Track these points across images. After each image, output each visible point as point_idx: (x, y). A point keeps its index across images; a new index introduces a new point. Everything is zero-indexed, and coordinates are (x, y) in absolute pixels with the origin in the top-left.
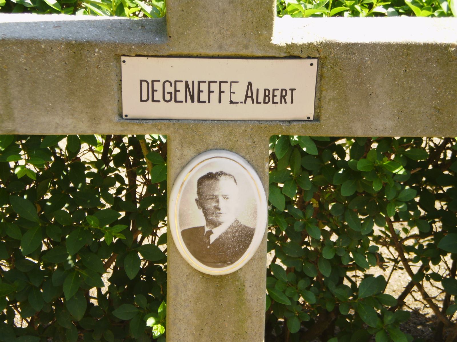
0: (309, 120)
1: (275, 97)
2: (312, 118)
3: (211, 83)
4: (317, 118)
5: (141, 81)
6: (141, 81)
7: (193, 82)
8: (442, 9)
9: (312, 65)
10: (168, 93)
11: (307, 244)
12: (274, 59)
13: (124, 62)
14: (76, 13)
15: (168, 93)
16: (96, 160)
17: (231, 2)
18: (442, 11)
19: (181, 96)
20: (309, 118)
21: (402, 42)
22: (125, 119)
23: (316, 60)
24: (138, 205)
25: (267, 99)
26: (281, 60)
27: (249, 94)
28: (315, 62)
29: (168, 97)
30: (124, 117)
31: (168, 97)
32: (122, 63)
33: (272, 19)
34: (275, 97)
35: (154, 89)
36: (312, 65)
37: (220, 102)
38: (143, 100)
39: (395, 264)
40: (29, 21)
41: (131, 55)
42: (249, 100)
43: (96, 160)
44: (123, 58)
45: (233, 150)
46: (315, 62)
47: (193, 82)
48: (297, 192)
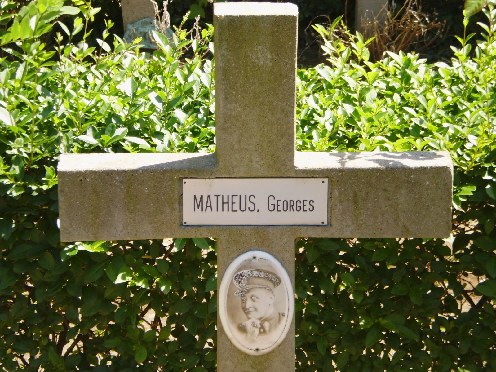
2: (326, 223)
4: (330, 224)
9: (323, 182)
10: (272, 204)
15: (272, 204)
17: (495, 139)
20: (323, 223)
21: (328, 167)
22: (185, 226)
24: (418, 277)
25: (225, 205)
26: (309, 179)
27: (209, 205)
28: (326, 180)
29: (298, 209)
30: (184, 224)
31: (271, 208)
32: (183, 183)
33: (293, 152)
36: (323, 182)
37: (217, 211)
39: (81, 347)
41: (315, 176)
42: (209, 209)
44: (184, 180)
45: (252, 249)
46: (326, 180)
48: (448, 286)
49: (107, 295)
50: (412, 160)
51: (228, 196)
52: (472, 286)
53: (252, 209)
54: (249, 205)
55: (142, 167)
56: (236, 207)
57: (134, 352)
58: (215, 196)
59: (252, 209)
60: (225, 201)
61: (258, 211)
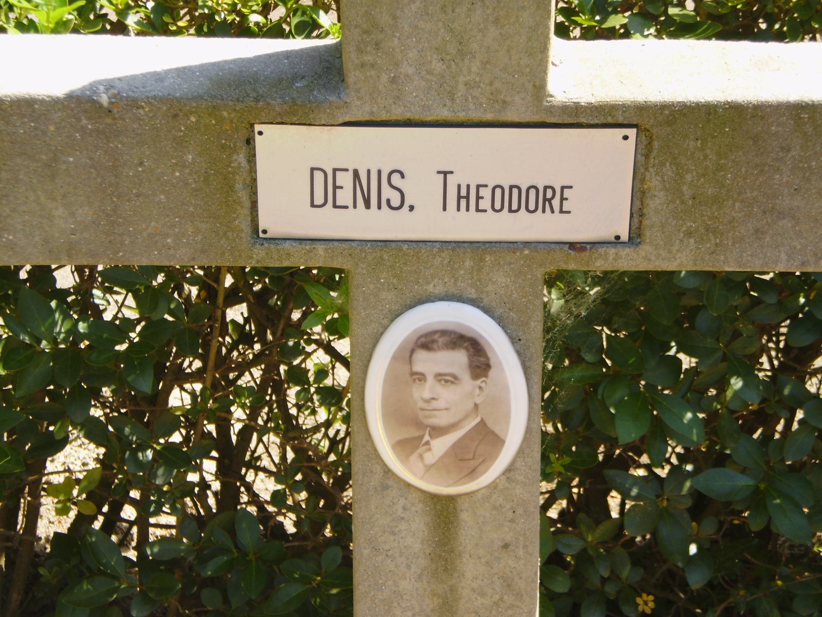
0: (620, 241)
1: (564, 201)
2: (625, 237)
3: (565, 190)
4: (636, 236)
5: (313, 170)
6: (313, 170)
7: (369, 171)
8: (323, 27)
9: (626, 138)
11: (271, 396)
12: (571, 128)
13: (260, 133)
14: (279, 18)
16: (130, 294)
18: (325, 29)
19: (345, 197)
20: (618, 238)
23: (634, 131)
24: (682, 376)
25: (463, 202)
30: (261, 235)
33: (549, 39)
34: (564, 201)
35: (338, 184)
36: (626, 138)
38: (315, 204)
40: (199, 38)
43: (130, 294)
46: (632, 132)
47: (369, 171)
49: (637, 306)
50: (551, 70)
51: (459, 186)
52: (183, 402)
53: (396, 202)
54: (387, 192)
55: (106, 80)
56: (485, 204)
57: (348, 506)
58: (439, 172)
59: (396, 202)
60: (463, 193)
61: (412, 208)
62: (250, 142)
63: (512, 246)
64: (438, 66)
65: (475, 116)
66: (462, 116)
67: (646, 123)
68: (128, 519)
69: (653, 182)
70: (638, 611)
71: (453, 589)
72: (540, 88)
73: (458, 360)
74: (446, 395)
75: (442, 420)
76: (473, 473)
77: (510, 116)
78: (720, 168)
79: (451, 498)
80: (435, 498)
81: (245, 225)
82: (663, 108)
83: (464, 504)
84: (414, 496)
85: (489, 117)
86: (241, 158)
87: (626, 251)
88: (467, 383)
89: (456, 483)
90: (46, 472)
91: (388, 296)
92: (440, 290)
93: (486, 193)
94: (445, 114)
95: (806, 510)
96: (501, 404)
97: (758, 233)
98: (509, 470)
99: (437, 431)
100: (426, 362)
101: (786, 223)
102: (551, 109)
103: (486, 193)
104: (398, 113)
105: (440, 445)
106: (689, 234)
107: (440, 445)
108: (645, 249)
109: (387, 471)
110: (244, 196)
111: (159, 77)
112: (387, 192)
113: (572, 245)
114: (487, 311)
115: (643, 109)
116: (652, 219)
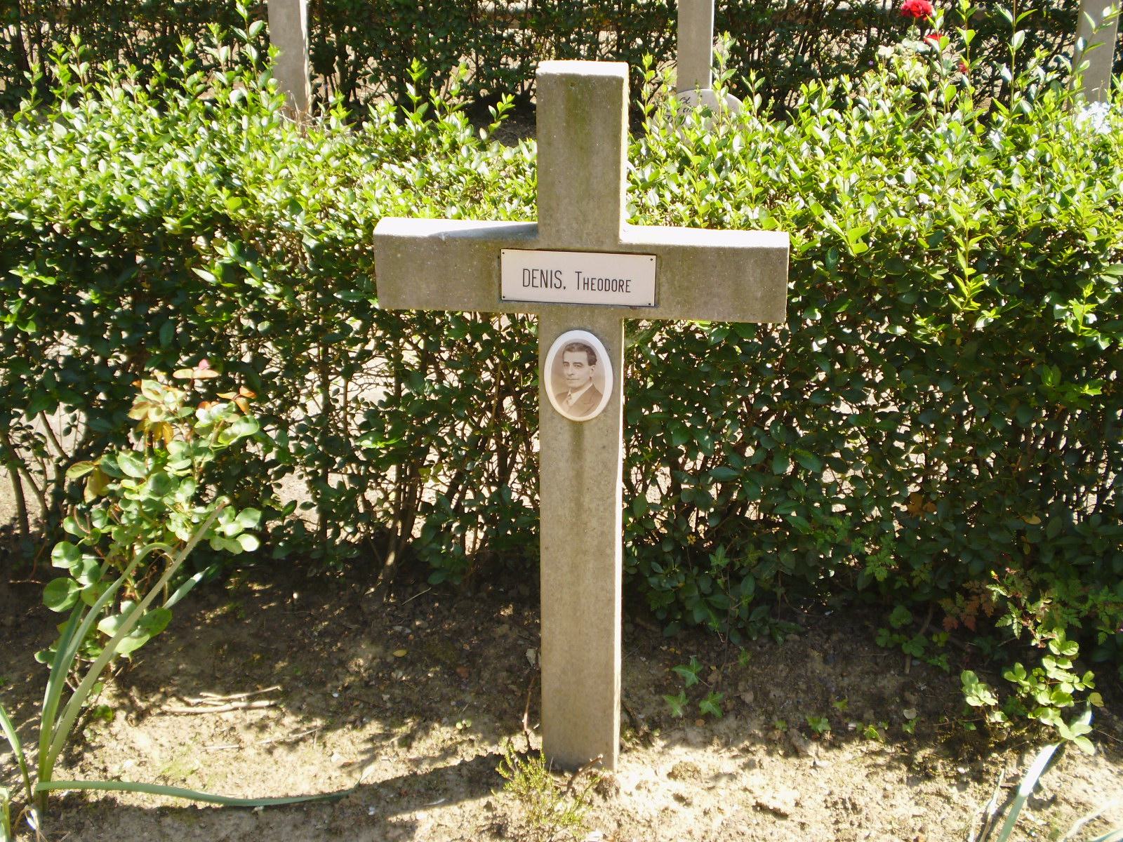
4: (657, 304)
19: (537, 282)
54: (555, 281)
56: (595, 287)
62: (499, 257)
63: (607, 306)
64: (575, 225)
65: (591, 247)
66: (585, 247)
67: (660, 253)
68: (9, 475)
69: (663, 279)
70: (1027, 34)
71: (581, 467)
72: (616, 236)
73: (582, 357)
74: (578, 373)
75: (577, 384)
76: (588, 411)
77: (605, 248)
78: (689, 274)
79: (581, 423)
80: (573, 423)
81: (496, 294)
82: (666, 247)
83: (586, 426)
84: (565, 422)
85: (596, 248)
86: (495, 264)
87: (652, 310)
88: (587, 368)
89: (582, 415)
90: (48, 417)
91: (555, 327)
92: (576, 325)
93: (595, 282)
94: (578, 246)
95: (817, 504)
96: (601, 378)
97: (706, 303)
98: (605, 411)
99: (576, 389)
100: (571, 357)
101: (716, 300)
102: (621, 246)
103: (595, 282)
104: (559, 246)
105: (575, 396)
106: (678, 303)
107: (575, 396)
108: (661, 309)
109: (554, 410)
110: (496, 280)
111: (465, 232)
112: (555, 281)
113: (631, 307)
114: (601, 340)
115: (658, 247)
116: (663, 296)
